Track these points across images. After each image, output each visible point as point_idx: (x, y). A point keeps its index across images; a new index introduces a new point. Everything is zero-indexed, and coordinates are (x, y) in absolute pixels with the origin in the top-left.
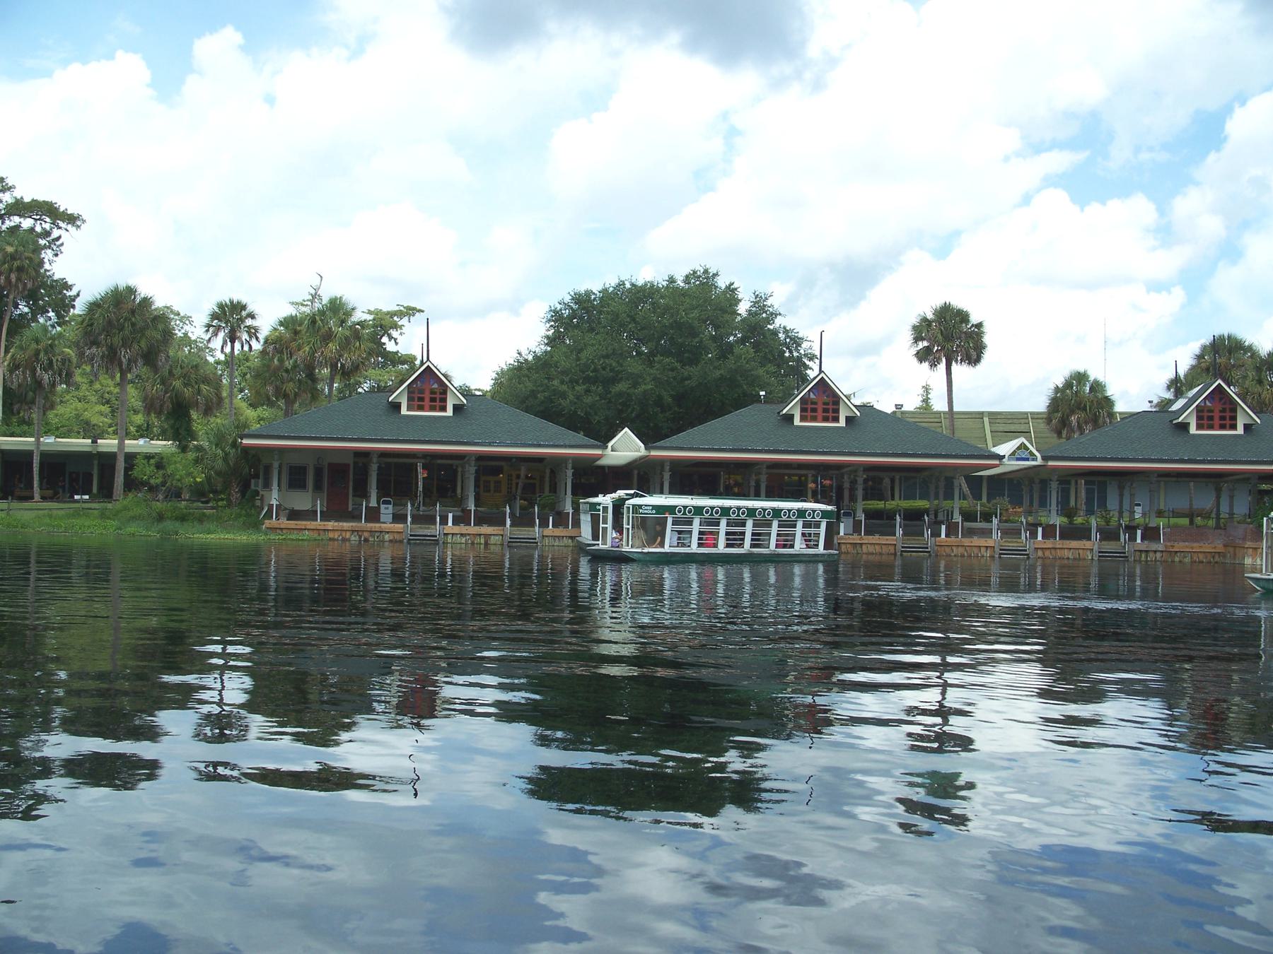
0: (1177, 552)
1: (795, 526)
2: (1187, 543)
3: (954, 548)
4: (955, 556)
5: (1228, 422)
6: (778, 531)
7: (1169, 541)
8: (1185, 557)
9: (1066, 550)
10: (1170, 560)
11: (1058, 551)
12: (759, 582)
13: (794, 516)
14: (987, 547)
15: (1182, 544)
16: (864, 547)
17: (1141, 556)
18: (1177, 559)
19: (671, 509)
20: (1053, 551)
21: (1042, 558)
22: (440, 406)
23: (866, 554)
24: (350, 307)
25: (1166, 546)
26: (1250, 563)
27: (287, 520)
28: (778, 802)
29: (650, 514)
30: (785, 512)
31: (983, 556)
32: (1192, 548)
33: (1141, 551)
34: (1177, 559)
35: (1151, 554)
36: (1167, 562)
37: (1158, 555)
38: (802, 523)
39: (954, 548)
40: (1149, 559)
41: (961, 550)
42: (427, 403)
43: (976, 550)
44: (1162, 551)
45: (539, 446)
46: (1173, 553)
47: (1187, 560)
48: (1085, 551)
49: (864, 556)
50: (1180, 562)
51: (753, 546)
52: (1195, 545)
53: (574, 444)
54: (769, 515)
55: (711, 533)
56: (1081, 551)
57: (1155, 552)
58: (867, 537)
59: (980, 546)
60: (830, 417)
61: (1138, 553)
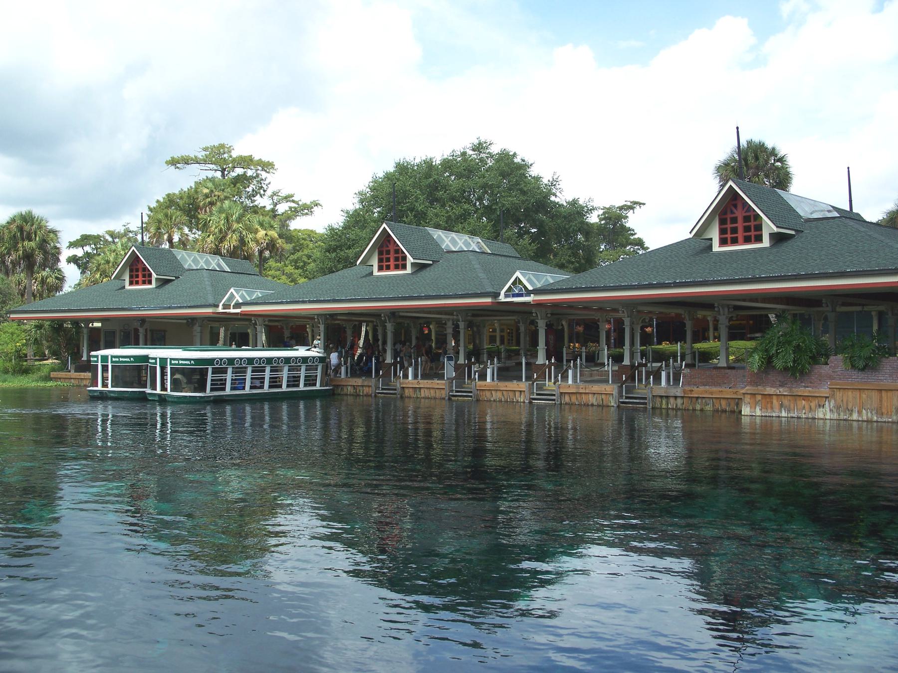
0: (697, 398)
1: (264, 371)
2: (707, 387)
3: (493, 393)
4: (494, 401)
5: (753, 233)
6: (270, 375)
7: (689, 384)
8: (707, 404)
9: (590, 396)
10: (691, 408)
11: (583, 396)
12: (824, 423)
13: (299, 362)
14: (521, 391)
15: (702, 388)
16: (422, 391)
17: (661, 403)
18: (698, 407)
19: (210, 361)
20: (578, 396)
21: (569, 404)
22: (732, 238)
23: (424, 398)
24: (511, 153)
25: (684, 392)
26: (749, 414)
27: (75, 372)
28: (27, 566)
29: (188, 365)
30: (276, 360)
31: (517, 402)
32: (712, 393)
33: (661, 397)
34: (698, 407)
35: (672, 400)
36: (688, 410)
37: (679, 401)
38: (305, 367)
39: (493, 393)
40: (670, 406)
41: (499, 394)
42: (740, 235)
43: (511, 394)
44: (682, 397)
45: (170, 308)
46: (694, 400)
47: (709, 408)
48: (608, 396)
49: (423, 400)
50: (702, 410)
51: (270, 387)
52: (714, 389)
53: (199, 304)
54: (263, 363)
55: (221, 380)
56: (603, 396)
57: (676, 397)
58: (422, 381)
59: (515, 391)
60: (729, 239)
61: (659, 399)
